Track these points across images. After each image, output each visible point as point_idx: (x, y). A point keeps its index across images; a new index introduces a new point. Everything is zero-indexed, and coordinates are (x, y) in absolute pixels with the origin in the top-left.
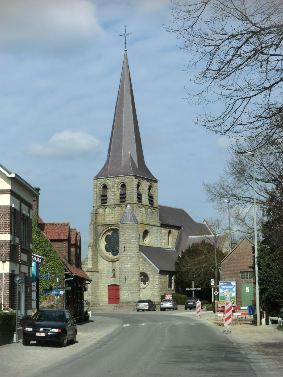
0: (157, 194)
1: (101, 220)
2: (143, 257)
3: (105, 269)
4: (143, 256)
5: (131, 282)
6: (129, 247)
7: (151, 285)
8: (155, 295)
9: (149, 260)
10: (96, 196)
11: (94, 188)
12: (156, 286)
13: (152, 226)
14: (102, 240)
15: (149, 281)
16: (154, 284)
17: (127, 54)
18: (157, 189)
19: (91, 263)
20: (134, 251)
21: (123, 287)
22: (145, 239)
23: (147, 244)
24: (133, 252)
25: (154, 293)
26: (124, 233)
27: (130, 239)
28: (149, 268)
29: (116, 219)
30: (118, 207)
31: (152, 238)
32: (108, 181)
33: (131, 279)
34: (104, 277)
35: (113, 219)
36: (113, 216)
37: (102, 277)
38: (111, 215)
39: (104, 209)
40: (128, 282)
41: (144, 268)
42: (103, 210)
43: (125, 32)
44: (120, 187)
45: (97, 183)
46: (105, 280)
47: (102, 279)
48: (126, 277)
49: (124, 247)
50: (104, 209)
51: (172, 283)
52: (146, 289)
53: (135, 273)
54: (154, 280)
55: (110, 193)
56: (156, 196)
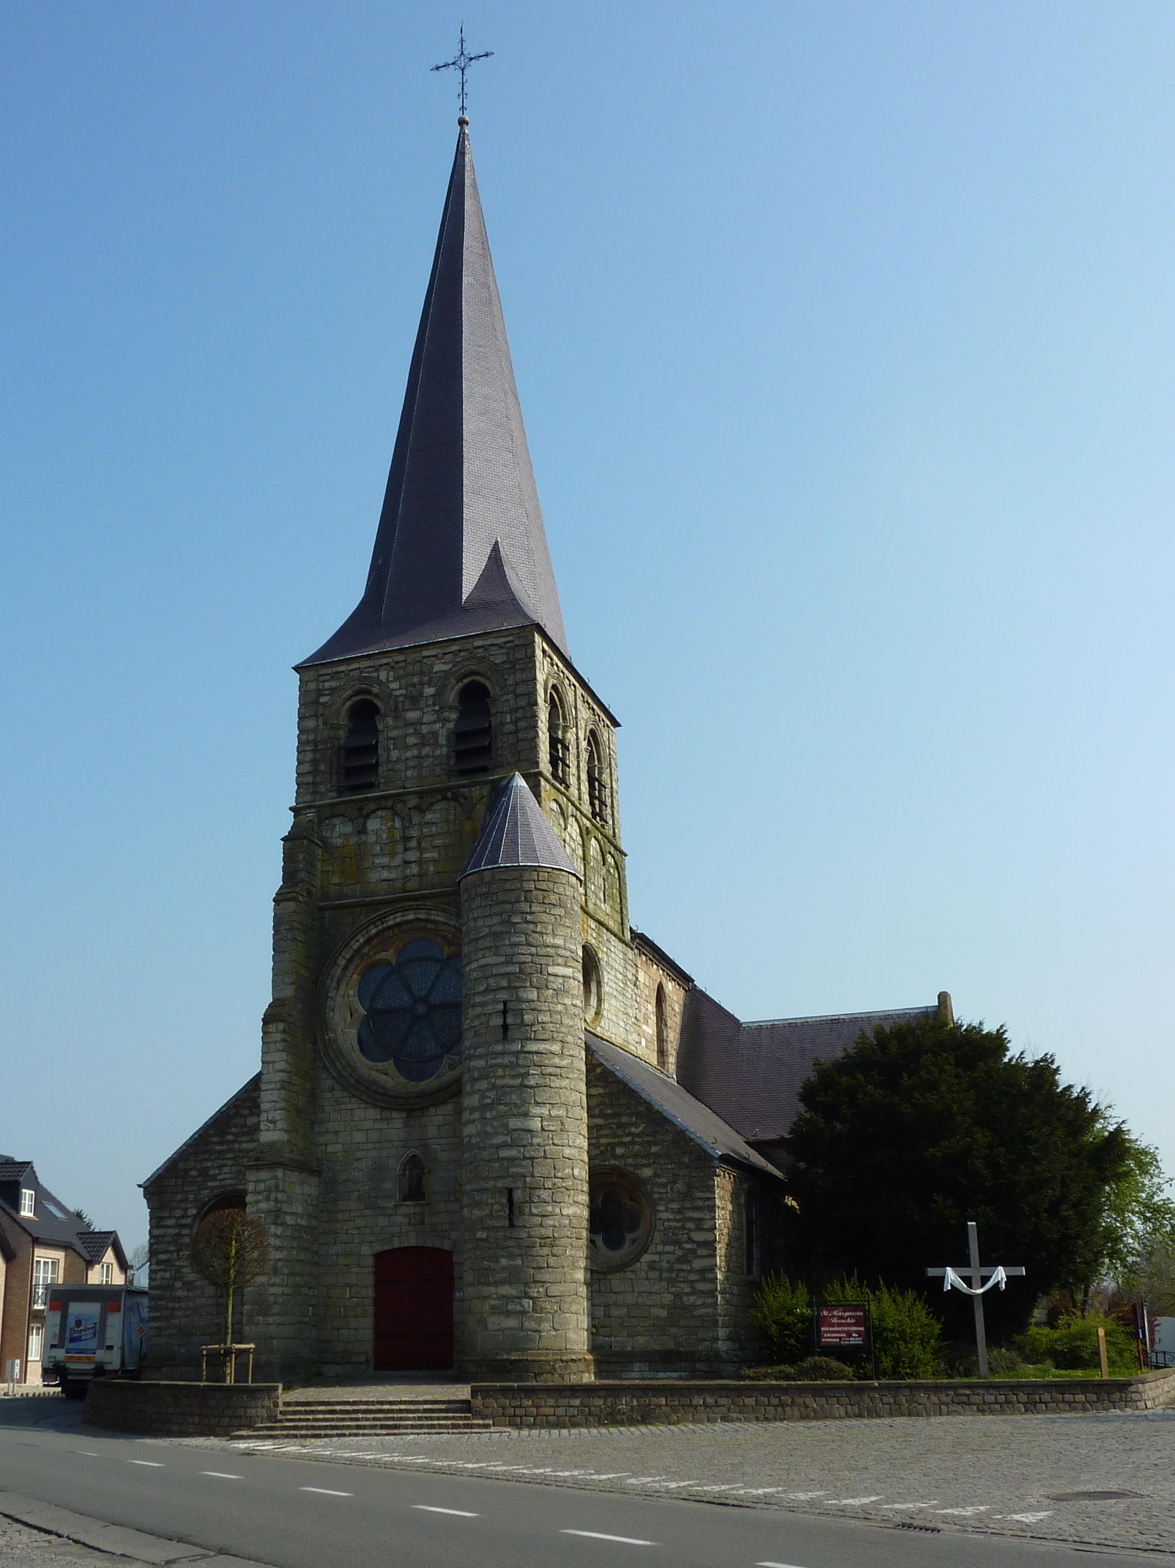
3: (358, 1154)
7: (669, 1248)
8: (697, 1313)
14: (341, 992)
26: (503, 922)
28: (650, 1144)
29: (432, 869)
32: (383, 675)
38: (400, 848)
41: (613, 1146)
44: (452, 697)
45: (318, 690)
49: (501, 1007)
52: (629, 1275)
54: (690, 1219)
55: (394, 733)
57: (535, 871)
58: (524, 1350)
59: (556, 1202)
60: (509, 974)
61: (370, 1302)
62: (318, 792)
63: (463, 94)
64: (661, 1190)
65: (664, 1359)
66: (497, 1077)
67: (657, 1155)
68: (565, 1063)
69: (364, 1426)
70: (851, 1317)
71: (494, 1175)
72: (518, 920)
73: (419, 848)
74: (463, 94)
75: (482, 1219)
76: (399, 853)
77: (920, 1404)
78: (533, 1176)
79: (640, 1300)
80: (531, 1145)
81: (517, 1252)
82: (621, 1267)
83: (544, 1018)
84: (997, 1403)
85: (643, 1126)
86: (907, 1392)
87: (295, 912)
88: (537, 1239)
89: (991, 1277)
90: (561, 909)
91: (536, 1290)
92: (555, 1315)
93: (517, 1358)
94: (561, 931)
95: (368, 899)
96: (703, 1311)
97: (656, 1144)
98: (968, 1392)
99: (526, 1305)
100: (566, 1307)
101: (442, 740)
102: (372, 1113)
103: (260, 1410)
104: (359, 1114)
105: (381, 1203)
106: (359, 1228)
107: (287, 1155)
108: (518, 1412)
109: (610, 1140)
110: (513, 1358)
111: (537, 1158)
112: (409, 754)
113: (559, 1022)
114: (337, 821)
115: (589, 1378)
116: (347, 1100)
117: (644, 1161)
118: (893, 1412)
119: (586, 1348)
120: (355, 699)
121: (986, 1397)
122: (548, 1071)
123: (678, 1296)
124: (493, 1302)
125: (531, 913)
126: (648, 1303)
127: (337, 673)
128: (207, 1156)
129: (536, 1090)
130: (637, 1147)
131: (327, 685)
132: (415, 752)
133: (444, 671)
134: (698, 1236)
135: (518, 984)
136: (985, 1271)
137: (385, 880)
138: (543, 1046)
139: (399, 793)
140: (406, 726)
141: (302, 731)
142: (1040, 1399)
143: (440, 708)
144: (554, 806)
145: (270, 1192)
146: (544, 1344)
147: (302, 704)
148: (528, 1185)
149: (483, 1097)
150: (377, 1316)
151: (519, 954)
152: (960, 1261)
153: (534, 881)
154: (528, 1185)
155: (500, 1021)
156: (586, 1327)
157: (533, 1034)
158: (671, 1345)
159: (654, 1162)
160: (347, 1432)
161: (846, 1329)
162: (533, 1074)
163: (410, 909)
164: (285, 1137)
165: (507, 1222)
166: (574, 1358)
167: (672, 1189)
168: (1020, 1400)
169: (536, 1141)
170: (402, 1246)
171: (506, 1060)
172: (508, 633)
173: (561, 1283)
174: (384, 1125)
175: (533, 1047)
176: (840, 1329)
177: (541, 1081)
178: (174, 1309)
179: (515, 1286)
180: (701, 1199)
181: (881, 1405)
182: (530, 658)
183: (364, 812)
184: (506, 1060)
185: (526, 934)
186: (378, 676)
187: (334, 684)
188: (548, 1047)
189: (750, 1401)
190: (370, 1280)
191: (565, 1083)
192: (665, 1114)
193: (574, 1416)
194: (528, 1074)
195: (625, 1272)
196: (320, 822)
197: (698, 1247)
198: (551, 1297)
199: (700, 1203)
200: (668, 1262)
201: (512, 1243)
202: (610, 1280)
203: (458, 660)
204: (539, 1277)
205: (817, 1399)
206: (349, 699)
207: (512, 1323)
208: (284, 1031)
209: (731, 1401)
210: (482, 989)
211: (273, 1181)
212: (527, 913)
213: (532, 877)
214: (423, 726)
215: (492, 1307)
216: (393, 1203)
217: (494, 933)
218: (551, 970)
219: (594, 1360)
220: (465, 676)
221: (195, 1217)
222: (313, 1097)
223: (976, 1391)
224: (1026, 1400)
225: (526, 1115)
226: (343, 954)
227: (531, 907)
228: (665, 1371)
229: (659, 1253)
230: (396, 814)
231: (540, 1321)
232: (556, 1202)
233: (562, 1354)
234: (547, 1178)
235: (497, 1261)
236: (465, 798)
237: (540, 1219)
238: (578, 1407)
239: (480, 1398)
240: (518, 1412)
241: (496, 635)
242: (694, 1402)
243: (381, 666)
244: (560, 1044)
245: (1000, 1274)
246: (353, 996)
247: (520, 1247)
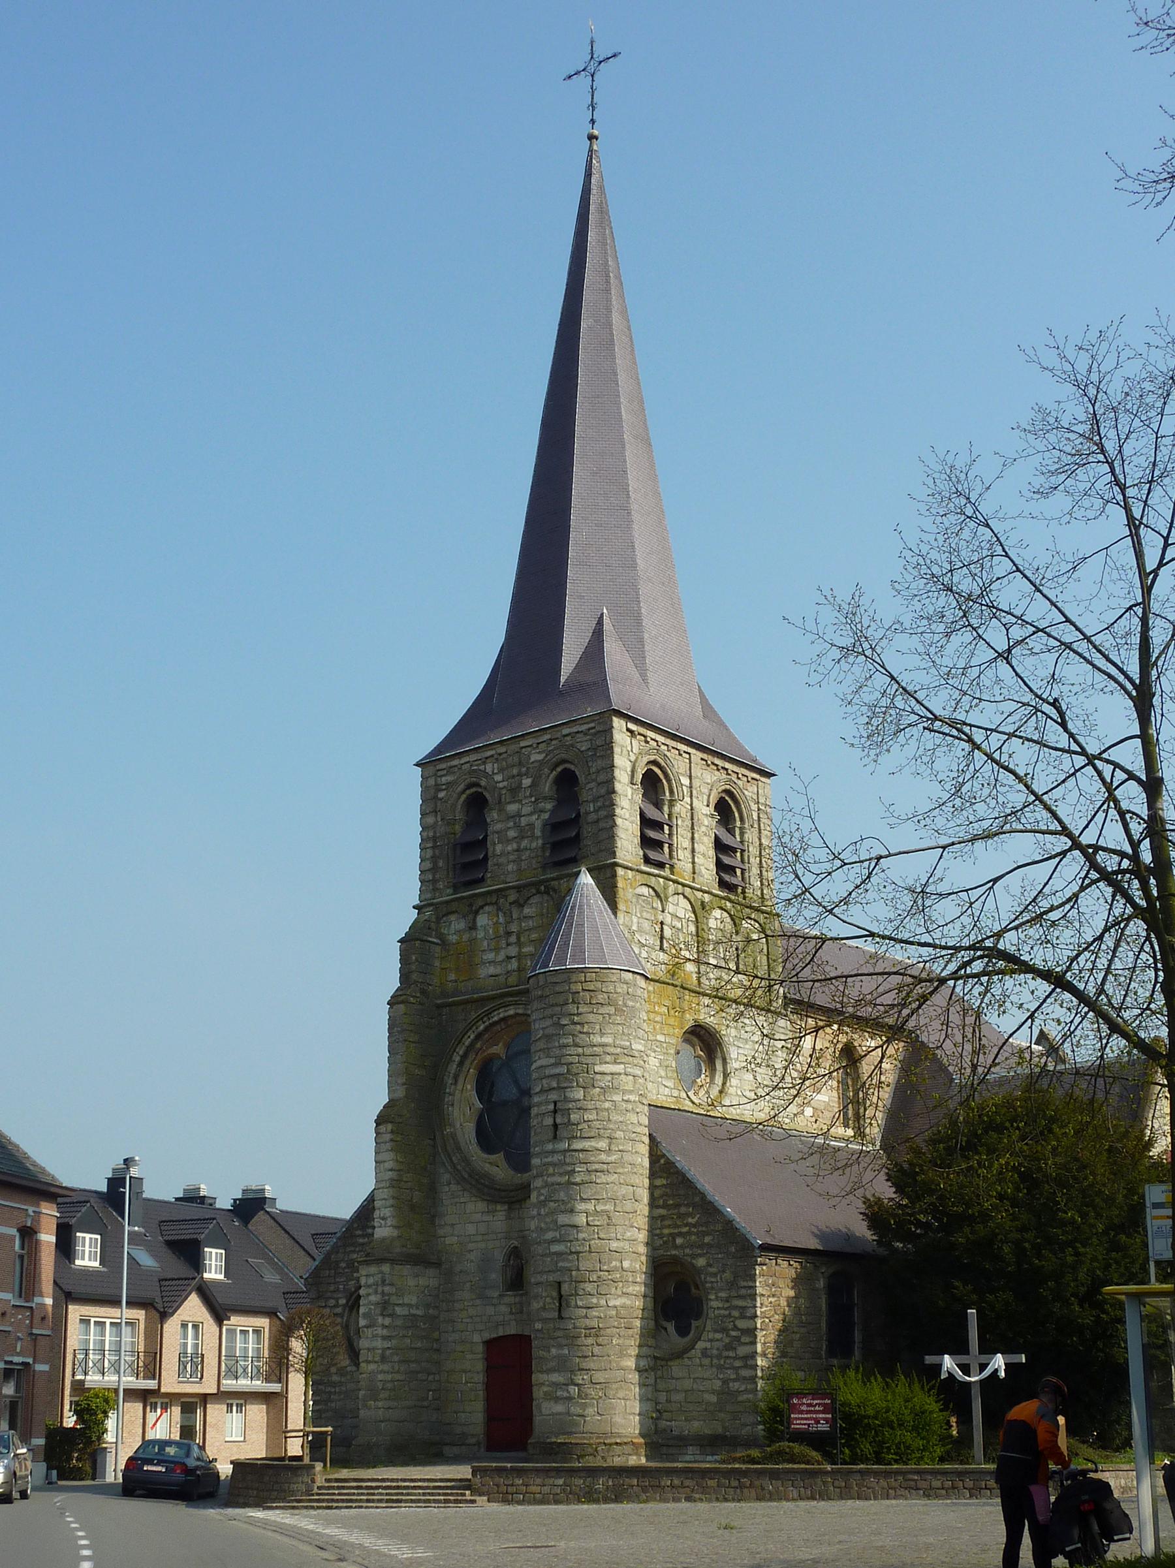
3: (471, 1246)
7: (718, 1336)
8: (740, 1398)
14: (460, 1087)
19: (387, 1212)
21: (547, 1349)
25: (735, 1386)
38: (503, 943)
39: (471, 917)
41: (673, 1236)
42: (461, 925)
46: (472, 1311)
49: (551, 1107)
50: (471, 917)
51: (462, 896)
52: (686, 1361)
54: (736, 1308)
55: (498, 826)
57: (583, 972)
58: (571, 1433)
59: (601, 1294)
60: (559, 1074)
61: (480, 1387)
62: (437, 889)
63: (593, 106)
64: (713, 1280)
65: (712, 1443)
66: (549, 1175)
67: (709, 1245)
68: (613, 1158)
69: (373, 1500)
70: (819, 1405)
71: (547, 1270)
72: (566, 1022)
73: (519, 943)
74: (593, 106)
76: (502, 948)
77: (868, 1488)
78: (578, 1270)
79: (695, 1386)
80: (577, 1240)
81: (564, 1342)
82: (680, 1355)
83: (590, 1116)
84: (943, 1488)
85: (698, 1216)
86: (858, 1476)
87: (405, 1014)
88: (583, 1330)
89: (989, 1364)
90: (610, 1008)
91: (581, 1377)
92: (600, 1401)
93: (563, 1441)
94: (609, 1029)
95: (475, 996)
96: (745, 1397)
98: (916, 1478)
99: (572, 1392)
100: (611, 1393)
101: (538, 833)
102: (481, 1206)
103: (300, 1485)
104: (470, 1207)
107: (398, 1250)
108: (510, 1489)
109: (672, 1231)
110: (559, 1441)
111: (582, 1252)
112: (509, 848)
113: (607, 1119)
114: (453, 917)
115: (639, 1460)
116: (461, 1193)
118: (843, 1495)
119: (637, 1432)
120: (468, 792)
121: (933, 1483)
122: (594, 1168)
123: (725, 1382)
124: (545, 1389)
125: (578, 1014)
126: (702, 1388)
127: (451, 767)
128: (353, 1249)
129: (581, 1186)
130: (693, 1237)
131: (444, 779)
132: (515, 846)
133: (540, 761)
134: (741, 1324)
135: (566, 1085)
136: (983, 1359)
137: (492, 976)
138: (589, 1143)
139: (498, 889)
140: (508, 819)
141: (425, 828)
142: (986, 1485)
143: (536, 800)
144: (645, 890)
145: (377, 1285)
146: (588, 1428)
147: (424, 800)
148: (574, 1279)
149: (540, 1194)
150: (488, 1400)
151: (567, 1055)
152: (959, 1348)
153: (582, 983)
154: (574, 1279)
155: (549, 1121)
156: (638, 1412)
157: (579, 1132)
158: (720, 1430)
159: (707, 1252)
160: (354, 1505)
161: (814, 1416)
162: (579, 1172)
163: (510, 1005)
164: (395, 1233)
165: (557, 1314)
166: (618, 1441)
167: (721, 1278)
168: (966, 1486)
169: (581, 1236)
170: (506, 1334)
171: (556, 1158)
172: (589, 720)
173: (606, 1370)
175: (578, 1145)
176: (809, 1416)
177: (586, 1178)
178: (330, 1393)
179: (563, 1374)
180: (745, 1287)
181: (832, 1488)
182: (608, 744)
183: (474, 908)
184: (556, 1158)
185: (573, 1035)
186: (485, 769)
187: (449, 778)
188: (593, 1144)
189: (712, 1483)
190: (480, 1366)
191: (612, 1178)
192: (716, 1204)
193: (557, 1494)
194: (573, 1171)
195: (683, 1358)
196: (438, 919)
197: (742, 1334)
198: (596, 1384)
199: (743, 1292)
200: (718, 1349)
201: (559, 1333)
202: (670, 1366)
203: (551, 748)
204: (584, 1365)
205: (773, 1482)
206: (463, 792)
207: (559, 1408)
208: (392, 1132)
209: (695, 1482)
210: (538, 1090)
211: (380, 1276)
212: (574, 1015)
213: (580, 979)
214: (522, 818)
215: (545, 1393)
216: (498, 1293)
217: (547, 1036)
218: (598, 1068)
219: (645, 1444)
220: (557, 765)
221: (344, 1306)
222: (432, 1190)
223: (924, 1477)
224: (972, 1486)
225: (572, 1211)
226: (457, 1050)
227: (578, 1008)
228: (713, 1455)
229: (711, 1341)
230: (499, 909)
231: (584, 1406)
232: (601, 1294)
233: (606, 1438)
234: (592, 1271)
235: (549, 1351)
236: (555, 890)
237: (584, 1311)
238: (561, 1486)
239: (479, 1477)
240: (510, 1489)
241: (580, 722)
242: (663, 1484)
243: (487, 758)
244: (607, 1141)
245: (999, 1362)
246: (470, 1091)
247: (567, 1337)
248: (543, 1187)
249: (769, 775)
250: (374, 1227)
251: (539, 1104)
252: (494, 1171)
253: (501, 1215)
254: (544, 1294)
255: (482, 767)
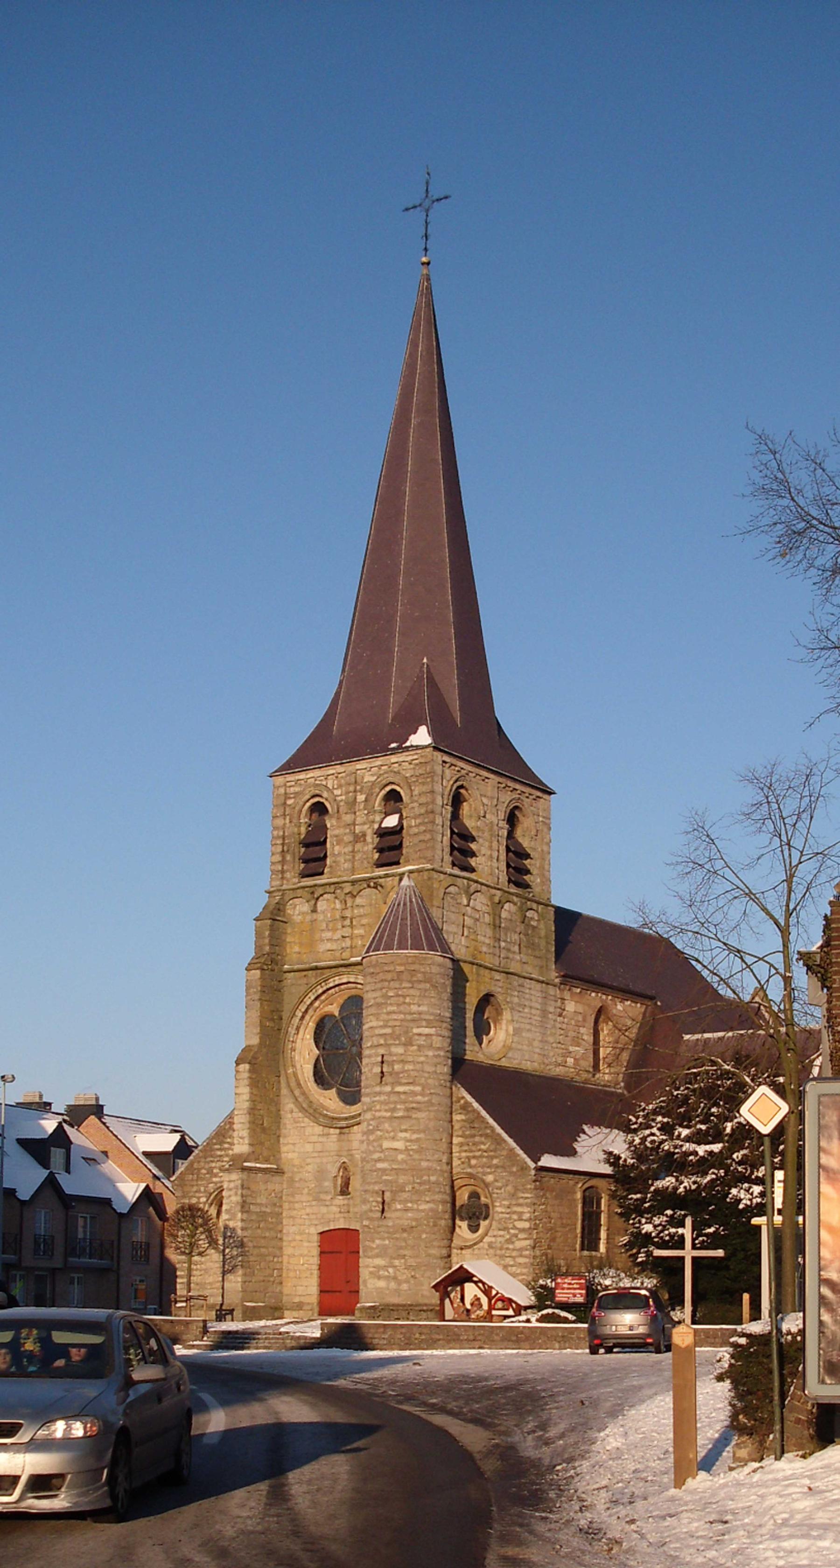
0: (545, 848)
1: (296, 949)
2: (466, 1107)
4: (467, 1102)
5: (407, 1219)
6: (402, 1061)
7: (501, 1233)
9: (491, 1121)
10: (279, 849)
11: (275, 817)
12: (521, 1236)
13: (521, 980)
14: (300, 1035)
15: (490, 1217)
16: (515, 1228)
17: (432, 278)
18: (550, 829)
19: (245, 1133)
20: (423, 1081)
22: (488, 1034)
23: (497, 1057)
24: (419, 1085)
27: (405, 1024)
28: (492, 1158)
29: (360, 942)
30: (368, 890)
31: (517, 1032)
33: (409, 1205)
34: (304, 1198)
35: (348, 943)
36: (347, 932)
37: (298, 1197)
39: (313, 902)
40: (397, 1215)
41: (469, 1158)
42: (306, 908)
43: (424, 195)
46: (308, 1210)
47: (297, 1206)
48: (387, 1195)
49: (379, 1059)
53: (425, 1178)
54: (515, 1212)
56: (545, 856)
60: (385, 1034)
66: (376, 1111)
67: (497, 1167)
75: (366, 1212)
97: (496, 1157)
105: (322, 1196)
106: (308, 1214)
117: (489, 1170)
124: (371, 1269)
131: (292, 790)
143: (369, 813)
149: (369, 1125)
155: (379, 1070)
174: (323, 1139)
187: (297, 789)
210: (369, 1045)
215: (371, 1273)
229: (494, 1236)
236: (382, 886)
248: (372, 1119)
249: (550, 793)
250: (232, 1144)
251: (370, 1056)
252: (327, 1103)
253: (334, 1138)
254: (371, 1199)
255: (324, 783)
